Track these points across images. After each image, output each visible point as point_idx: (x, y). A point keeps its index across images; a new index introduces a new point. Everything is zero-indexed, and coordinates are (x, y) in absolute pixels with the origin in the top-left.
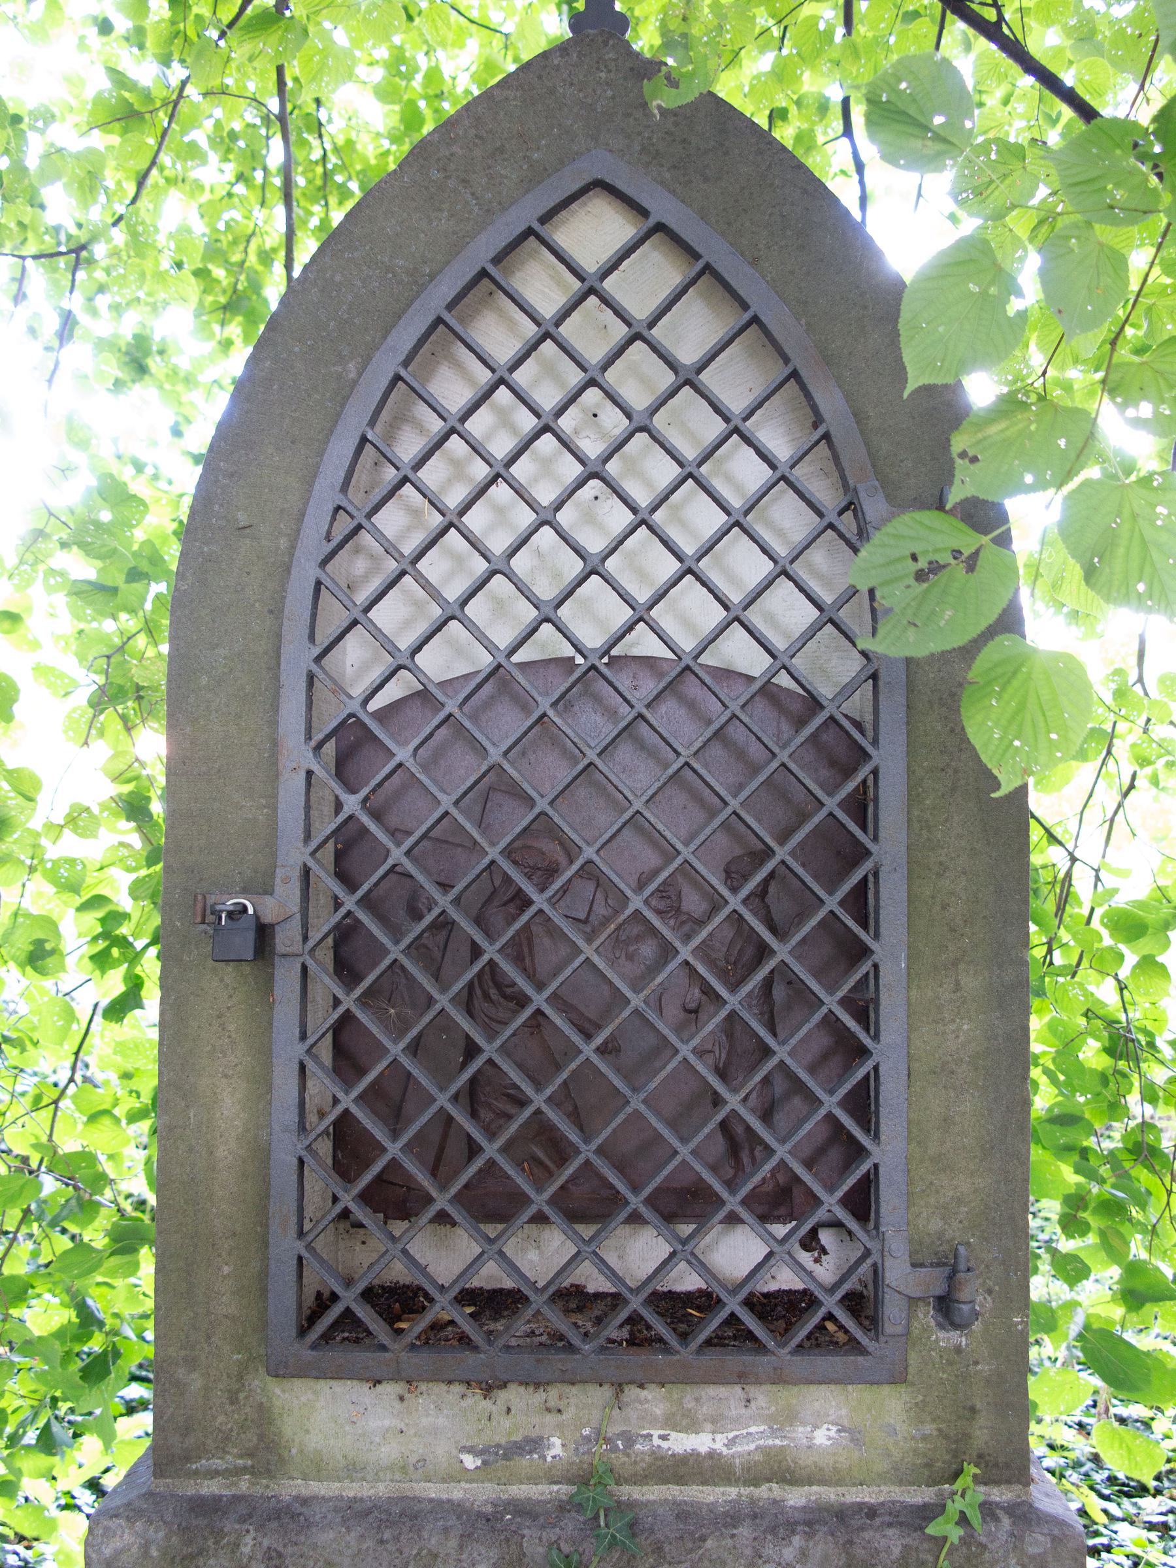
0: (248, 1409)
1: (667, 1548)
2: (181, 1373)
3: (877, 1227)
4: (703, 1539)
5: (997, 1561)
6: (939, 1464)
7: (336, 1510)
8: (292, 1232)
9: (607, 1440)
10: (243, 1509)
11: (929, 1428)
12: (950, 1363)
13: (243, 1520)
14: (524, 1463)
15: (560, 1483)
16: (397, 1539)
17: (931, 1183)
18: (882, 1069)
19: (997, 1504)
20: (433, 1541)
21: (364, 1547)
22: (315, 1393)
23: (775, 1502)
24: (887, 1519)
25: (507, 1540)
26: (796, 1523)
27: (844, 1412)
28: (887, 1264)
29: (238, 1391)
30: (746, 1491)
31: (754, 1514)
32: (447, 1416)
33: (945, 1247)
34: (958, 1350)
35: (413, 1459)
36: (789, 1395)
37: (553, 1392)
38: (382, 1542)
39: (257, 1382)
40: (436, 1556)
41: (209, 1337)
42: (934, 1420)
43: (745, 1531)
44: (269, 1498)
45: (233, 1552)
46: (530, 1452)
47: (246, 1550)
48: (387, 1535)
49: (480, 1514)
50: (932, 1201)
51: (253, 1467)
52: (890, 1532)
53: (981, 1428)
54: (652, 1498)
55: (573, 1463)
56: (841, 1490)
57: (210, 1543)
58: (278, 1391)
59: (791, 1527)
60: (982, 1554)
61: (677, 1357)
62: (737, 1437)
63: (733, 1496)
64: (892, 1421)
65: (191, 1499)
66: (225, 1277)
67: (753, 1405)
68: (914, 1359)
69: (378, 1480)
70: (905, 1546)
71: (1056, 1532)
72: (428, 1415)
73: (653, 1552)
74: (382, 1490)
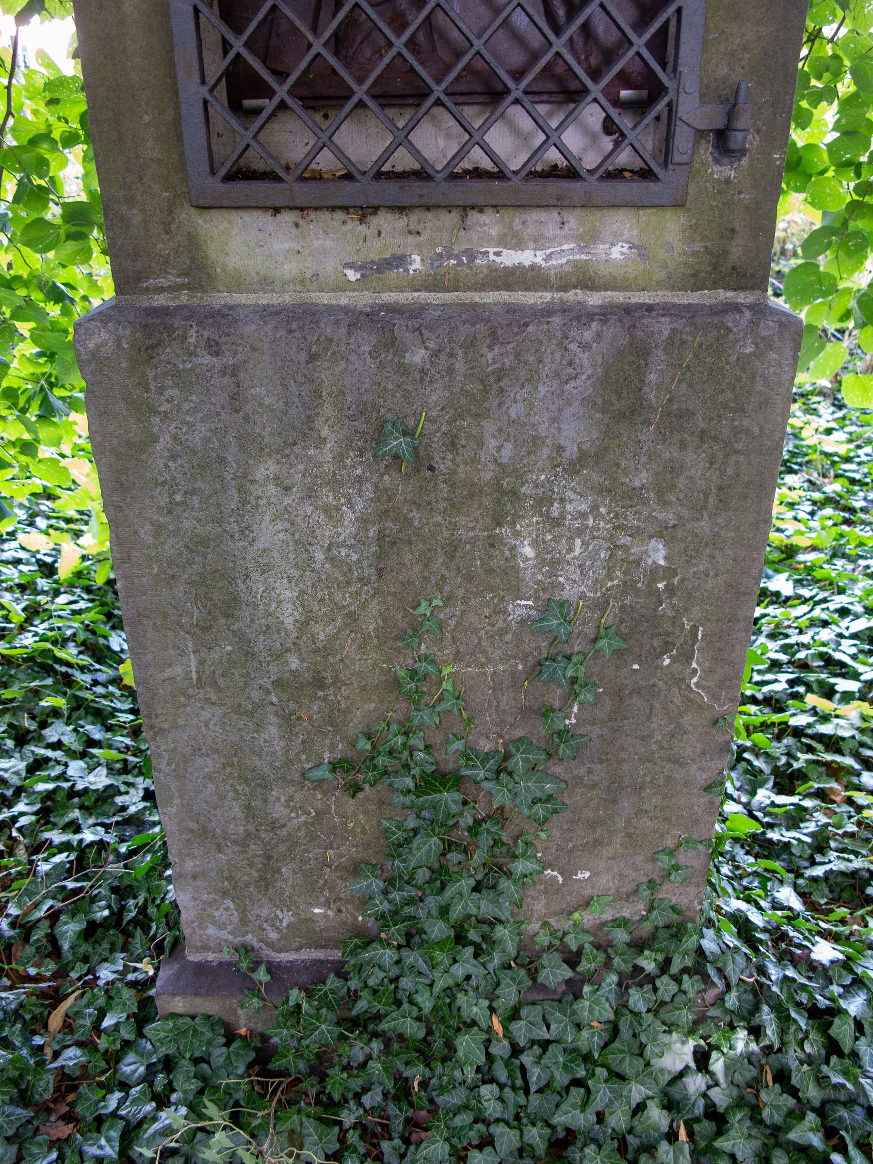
0: (179, 238)
1: (499, 332)
2: (124, 209)
3: (675, 70)
4: (526, 325)
5: (738, 341)
6: (703, 274)
7: (254, 312)
8: (197, 78)
9: (456, 257)
10: (185, 312)
11: (698, 246)
12: (720, 192)
13: (187, 319)
14: (393, 275)
15: (420, 290)
16: (302, 328)
17: (723, 31)
18: (684, 13)
19: (742, 304)
20: (329, 330)
21: (278, 335)
22: (229, 222)
23: (579, 302)
24: (661, 312)
25: (383, 328)
26: (595, 314)
27: (635, 232)
28: (681, 100)
29: (170, 223)
30: (557, 295)
31: (564, 309)
32: (333, 239)
33: (728, 91)
34: (727, 181)
35: (309, 275)
36: (594, 218)
37: (414, 217)
38: (291, 331)
39: (184, 215)
40: (331, 341)
41: (141, 178)
42: (702, 239)
43: (557, 320)
44: (204, 307)
45: (182, 342)
46: (397, 267)
47: (192, 340)
48: (294, 326)
49: (361, 313)
50: (722, 48)
51: (189, 283)
52: (663, 319)
53: (737, 245)
54: (488, 301)
55: (429, 275)
56: (628, 294)
57: (165, 336)
58: (200, 222)
59: (591, 317)
60: (728, 335)
61: (510, 183)
62: (552, 253)
63: (548, 299)
64: (671, 240)
65: (146, 309)
66: (146, 125)
67: (566, 227)
68: (692, 189)
69: (285, 291)
70: (673, 330)
71: (783, 320)
72: (318, 239)
73: (490, 335)
74: (287, 298)
